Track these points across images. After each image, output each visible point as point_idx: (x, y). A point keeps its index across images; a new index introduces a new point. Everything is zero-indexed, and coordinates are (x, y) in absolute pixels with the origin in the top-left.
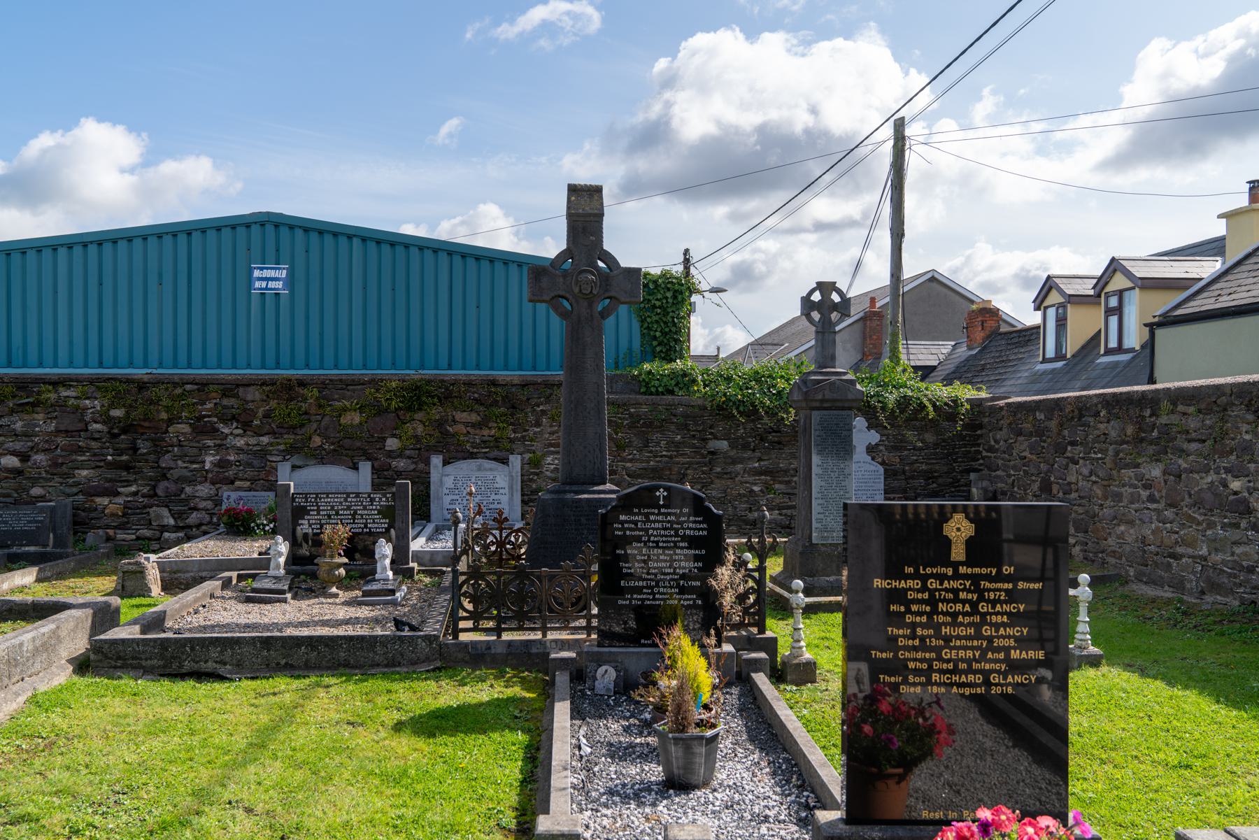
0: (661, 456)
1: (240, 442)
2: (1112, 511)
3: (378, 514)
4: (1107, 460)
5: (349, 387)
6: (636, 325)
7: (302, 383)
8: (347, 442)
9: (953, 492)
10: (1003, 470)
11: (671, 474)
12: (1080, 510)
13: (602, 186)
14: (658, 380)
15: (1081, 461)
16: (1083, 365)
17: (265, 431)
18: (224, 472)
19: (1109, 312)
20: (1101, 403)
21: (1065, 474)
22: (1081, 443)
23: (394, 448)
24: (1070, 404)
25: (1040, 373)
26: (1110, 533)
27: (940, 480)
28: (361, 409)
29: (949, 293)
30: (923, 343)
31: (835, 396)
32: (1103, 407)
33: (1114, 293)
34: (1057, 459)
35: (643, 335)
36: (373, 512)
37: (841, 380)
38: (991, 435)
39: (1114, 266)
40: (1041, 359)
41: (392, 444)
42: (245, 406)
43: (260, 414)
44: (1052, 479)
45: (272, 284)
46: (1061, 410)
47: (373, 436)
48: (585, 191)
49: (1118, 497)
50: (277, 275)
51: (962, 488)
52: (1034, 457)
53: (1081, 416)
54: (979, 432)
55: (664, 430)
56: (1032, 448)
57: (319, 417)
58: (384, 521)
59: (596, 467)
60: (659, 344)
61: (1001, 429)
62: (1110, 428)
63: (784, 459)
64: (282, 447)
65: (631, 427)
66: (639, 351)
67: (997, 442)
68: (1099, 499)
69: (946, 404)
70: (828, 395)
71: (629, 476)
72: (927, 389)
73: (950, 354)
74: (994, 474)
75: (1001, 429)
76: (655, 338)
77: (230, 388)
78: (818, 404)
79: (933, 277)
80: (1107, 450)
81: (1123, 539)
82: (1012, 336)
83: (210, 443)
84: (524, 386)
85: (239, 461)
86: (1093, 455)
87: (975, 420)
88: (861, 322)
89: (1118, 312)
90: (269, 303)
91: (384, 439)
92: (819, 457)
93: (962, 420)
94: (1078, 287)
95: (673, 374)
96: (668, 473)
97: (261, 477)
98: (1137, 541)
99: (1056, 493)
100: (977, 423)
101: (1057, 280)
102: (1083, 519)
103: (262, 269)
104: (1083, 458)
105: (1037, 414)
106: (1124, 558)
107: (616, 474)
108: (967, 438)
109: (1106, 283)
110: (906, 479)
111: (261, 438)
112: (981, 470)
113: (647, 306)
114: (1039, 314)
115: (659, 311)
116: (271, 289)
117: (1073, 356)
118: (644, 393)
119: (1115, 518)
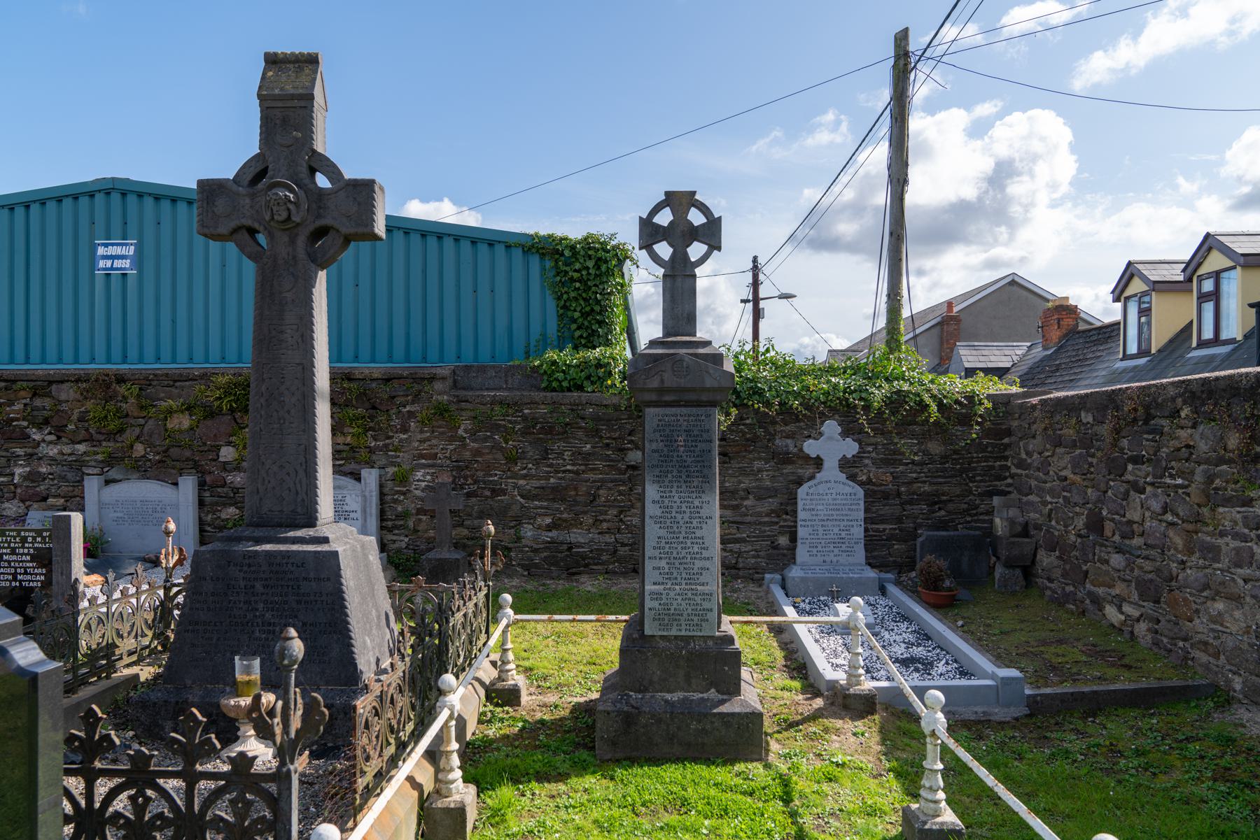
0: (564, 472)
1: (53, 451)
2: (1200, 574)
3: (31, 561)
4: (1193, 489)
5: (178, 384)
6: (551, 304)
7: (121, 379)
8: (174, 452)
9: (969, 522)
10: (1037, 495)
11: (577, 495)
12: (1148, 566)
13: (317, 55)
14: (563, 372)
15: (1149, 489)
16: (1171, 360)
17: (81, 437)
18: (35, 487)
19: (1203, 298)
20: (1181, 395)
21: (1123, 507)
22: (1149, 460)
23: (230, 458)
24: (1131, 399)
25: (1120, 370)
26: (1197, 611)
27: (951, 506)
28: (189, 409)
29: (1031, 296)
30: (995, 344)
31: (683, 383)
32: (1185, 402)
33: (1209, 275)
34: (1112, 483)
35: (561, 317)
36: (24, 558)
37: (696, 355)
38: (1021, 444)
39: (1209, 244)
40: (1121, 356)
41: (227, 453)
42: (59, 407)
43: (75, 417)
44: (1104, 513)
45: (118, 264)
46: (1117, 408)
47: (205, 444)
48: (290, 62)
49: (1212, 553)
50: (123, 253)
51: (981, 517)
52: (1078, 478)
53: (1148, 418)
54: (1006, 440)
55: (567, 438)
56: (1075, 465)
57: (142, 421)
58: (40, 571)
59: (299, 500)
60: (579, 328)
61: (1034, 437)
62: (1197, 437)
63: (731, 476)
64: (100, 457)
65: (525, 432)
66: (555, 336)
67: (1029, 454)
68: (1180, 552)
69: (957, 402)
70: (670, 380)
71: (522, 496)
72: (932, 382)
73: (1024, 356)
74: (1025, 499)
75: (1034, 437)
76: (574, 321)
77: (42, 386)
78: (654, 397)
79: (1013, 280)
80: (1192, 473)
81: (1222, 625)
82: (1091, 334)
83: (20, 451)
84: (388, 380)
85: (52, 474)
86: (1168, 481)
87: (1001, 424)
88: (939, 327)
89: (1214, 297)
90: (115, 285)
91: (217, 448)
92: (656, 486)
93: (978, 423)
94: (1165, 272)
95: (585, 364)
96: (573, 493)
97: (75, 493)
98: (1248, 633)
99: (1110, 534)
100: (1004, 427)
101: (1139, 267)
102: (1151, 581)
103: (106, 245)
104: (1152, 484)
105: (1083, 414)
106: (1222, 657)
107: (505, 495)
108: (989, 449)
109: (1199, 265)
110: (902, 504)
111: (78, 446)
112: (1009, 493)
113: (563, 280)
114: (1119, 305)
115: (578, 285)
116: (117, 269)
117: (1159, 351)
118: (545, 389)
119: (1206, 586)
